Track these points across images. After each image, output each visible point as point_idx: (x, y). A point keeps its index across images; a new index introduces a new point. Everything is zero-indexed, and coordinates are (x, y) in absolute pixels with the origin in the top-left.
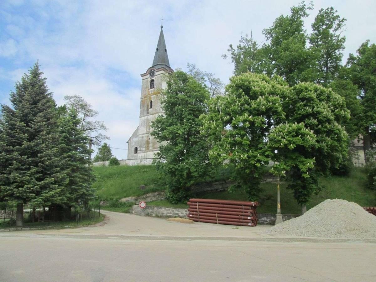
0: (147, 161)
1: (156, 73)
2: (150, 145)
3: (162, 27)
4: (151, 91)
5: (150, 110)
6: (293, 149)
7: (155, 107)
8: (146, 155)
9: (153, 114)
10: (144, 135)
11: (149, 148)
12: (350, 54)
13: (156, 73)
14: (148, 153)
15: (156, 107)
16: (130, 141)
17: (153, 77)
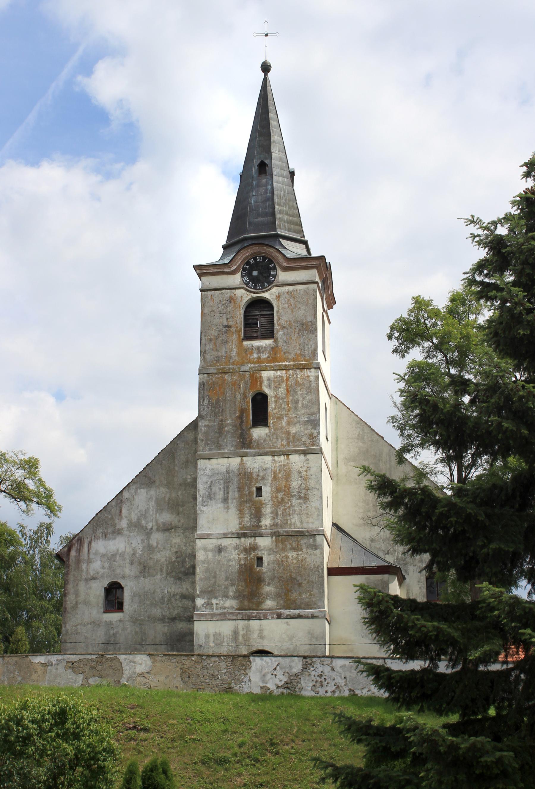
0: (333, 669)
1: (283, 276)
2: (267, 589)
3: (266, 68)
4: (259, 350)
5: (258, 433)
6: (463, 603)
7: (284, 423)
8: (248, 629)
9: (273, 454)
10: (225, 542)
11: (260, 603)
12: (414, 298)
13: (283, 276)
14: (255, 624)
15: (289, 423)
16: (79, 551)
17: (264, 289)
